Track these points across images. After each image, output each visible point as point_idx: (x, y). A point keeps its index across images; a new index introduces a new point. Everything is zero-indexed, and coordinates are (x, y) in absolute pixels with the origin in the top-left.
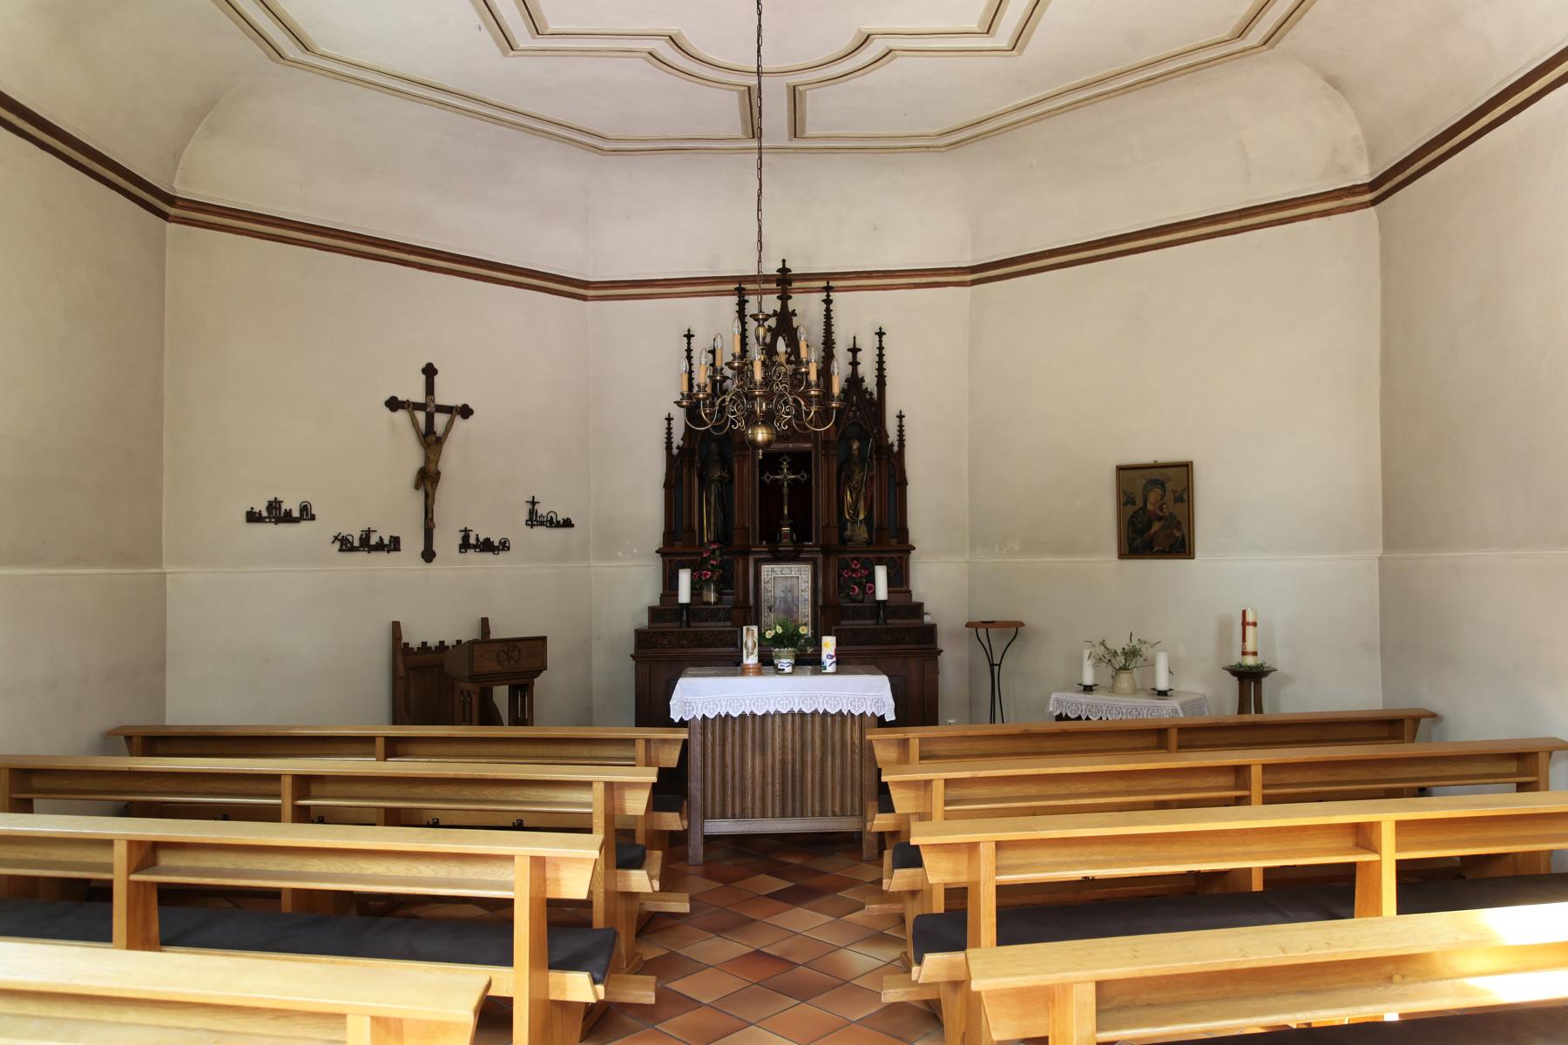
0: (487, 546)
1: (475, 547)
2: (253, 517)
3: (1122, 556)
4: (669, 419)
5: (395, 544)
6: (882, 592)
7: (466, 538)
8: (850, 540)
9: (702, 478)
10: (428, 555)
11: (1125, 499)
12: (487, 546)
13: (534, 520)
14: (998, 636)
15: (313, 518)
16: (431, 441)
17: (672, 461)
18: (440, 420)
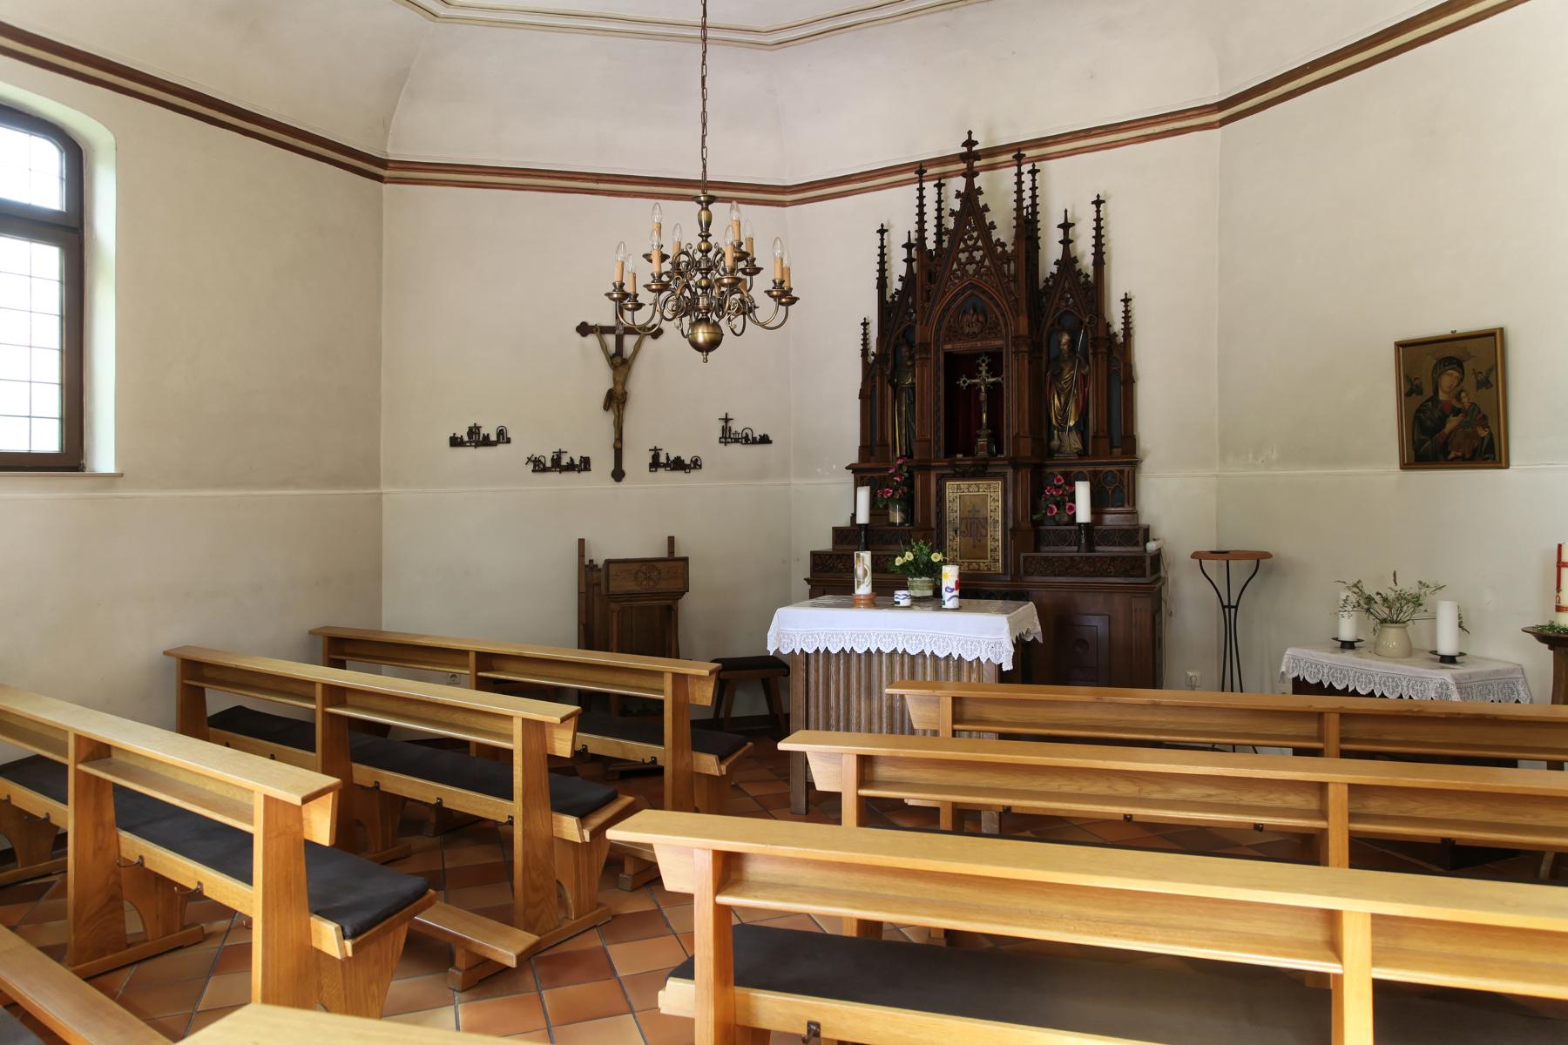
0: (677, 465)
1: (665, 466)
2: (455, 442)
3: (1405, 466)
4: (865, 324)
5: (585, 464)
6: (1083, 513)
7: (656, 457)
8: (1059, 450)
9: (895, 387)
10: (618, 474)
11: (1409, 387)
12: (677, 465)
13: (727, 437)
14: (1245, 569)
15: (509, 441)
16: (620, 363)
17: (867, 367)
18: (630, 341)
